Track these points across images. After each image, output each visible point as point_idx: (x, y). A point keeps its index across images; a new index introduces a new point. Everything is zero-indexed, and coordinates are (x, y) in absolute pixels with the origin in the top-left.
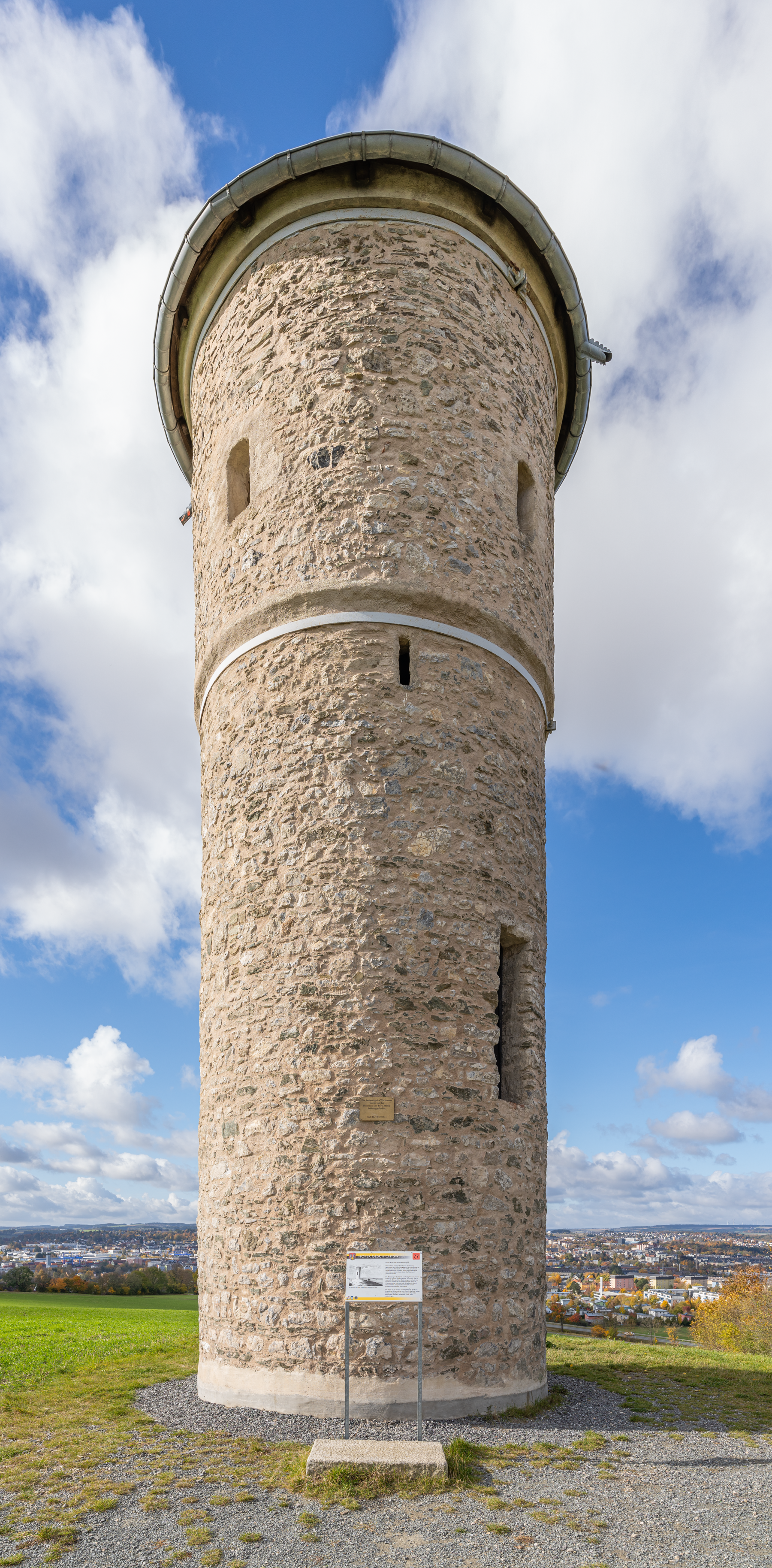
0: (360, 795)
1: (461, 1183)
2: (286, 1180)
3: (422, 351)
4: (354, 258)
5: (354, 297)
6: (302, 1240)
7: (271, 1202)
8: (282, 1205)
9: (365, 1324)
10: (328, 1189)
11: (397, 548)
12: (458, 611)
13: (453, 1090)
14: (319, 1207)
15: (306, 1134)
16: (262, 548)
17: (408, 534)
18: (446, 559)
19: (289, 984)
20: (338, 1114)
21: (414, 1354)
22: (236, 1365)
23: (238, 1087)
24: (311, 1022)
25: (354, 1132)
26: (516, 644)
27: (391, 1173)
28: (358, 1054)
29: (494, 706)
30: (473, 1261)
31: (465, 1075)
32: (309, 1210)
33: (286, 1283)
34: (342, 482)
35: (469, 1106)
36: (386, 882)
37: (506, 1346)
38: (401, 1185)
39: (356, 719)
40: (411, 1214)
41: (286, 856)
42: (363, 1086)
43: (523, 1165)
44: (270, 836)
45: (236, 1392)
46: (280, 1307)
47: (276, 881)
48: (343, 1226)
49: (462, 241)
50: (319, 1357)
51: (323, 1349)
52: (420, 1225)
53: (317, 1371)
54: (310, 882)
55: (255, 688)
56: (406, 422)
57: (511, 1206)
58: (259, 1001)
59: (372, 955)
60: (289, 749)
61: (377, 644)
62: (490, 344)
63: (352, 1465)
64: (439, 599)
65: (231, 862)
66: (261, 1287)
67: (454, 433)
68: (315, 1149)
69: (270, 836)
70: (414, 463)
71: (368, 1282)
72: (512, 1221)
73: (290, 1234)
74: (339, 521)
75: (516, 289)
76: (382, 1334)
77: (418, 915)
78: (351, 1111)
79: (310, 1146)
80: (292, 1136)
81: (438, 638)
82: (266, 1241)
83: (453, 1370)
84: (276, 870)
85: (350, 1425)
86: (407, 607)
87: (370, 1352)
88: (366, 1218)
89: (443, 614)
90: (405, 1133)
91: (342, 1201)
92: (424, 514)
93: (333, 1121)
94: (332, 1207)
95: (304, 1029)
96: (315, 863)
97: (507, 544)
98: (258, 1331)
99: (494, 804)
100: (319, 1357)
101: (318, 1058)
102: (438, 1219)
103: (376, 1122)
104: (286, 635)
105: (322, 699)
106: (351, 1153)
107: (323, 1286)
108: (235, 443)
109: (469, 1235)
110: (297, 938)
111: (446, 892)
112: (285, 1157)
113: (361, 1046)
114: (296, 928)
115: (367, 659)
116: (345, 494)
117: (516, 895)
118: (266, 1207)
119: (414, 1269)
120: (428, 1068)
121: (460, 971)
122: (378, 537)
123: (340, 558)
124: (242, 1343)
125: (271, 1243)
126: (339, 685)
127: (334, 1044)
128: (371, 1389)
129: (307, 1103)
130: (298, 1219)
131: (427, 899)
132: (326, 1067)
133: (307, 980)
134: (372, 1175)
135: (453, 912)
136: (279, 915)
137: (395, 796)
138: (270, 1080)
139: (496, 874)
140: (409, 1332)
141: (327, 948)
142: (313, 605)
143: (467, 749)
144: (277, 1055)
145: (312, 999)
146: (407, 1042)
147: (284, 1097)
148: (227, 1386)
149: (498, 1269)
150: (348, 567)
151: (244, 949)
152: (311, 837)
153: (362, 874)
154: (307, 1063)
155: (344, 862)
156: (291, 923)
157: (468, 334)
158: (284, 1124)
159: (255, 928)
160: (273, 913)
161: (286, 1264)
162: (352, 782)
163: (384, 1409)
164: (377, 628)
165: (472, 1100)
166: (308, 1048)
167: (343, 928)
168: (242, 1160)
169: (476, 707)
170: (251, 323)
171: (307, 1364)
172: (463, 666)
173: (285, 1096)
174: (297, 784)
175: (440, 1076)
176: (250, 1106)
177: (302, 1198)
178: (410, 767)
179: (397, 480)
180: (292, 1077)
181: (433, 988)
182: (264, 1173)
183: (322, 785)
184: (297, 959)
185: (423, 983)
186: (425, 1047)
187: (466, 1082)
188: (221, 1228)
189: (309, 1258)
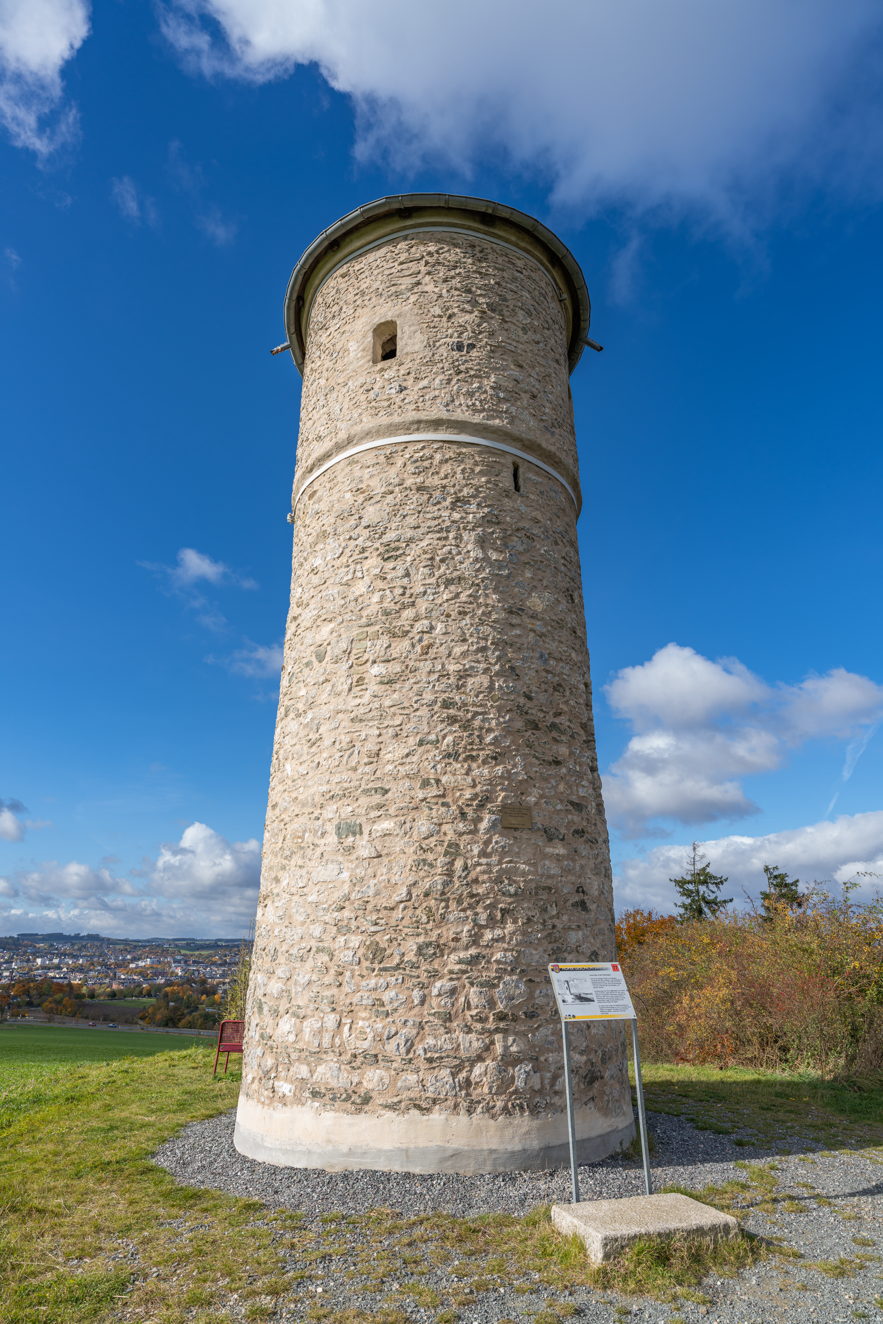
1: (583, 892)
3: (522, 312)
6: (442, 951)
7: (405, 908)
8: (418, 912)
9: (514, 1049)
10: (472, 896)
11: (513, 409)
12: (549, 456)
13: (572, 803)
14: (462, 914)
15: (449, 838)
16: (409, 383)
17: (519, 403)
18: (542, 424)
19: (428, 697)
20: (481, 819)
23: (363, 787)
24: (451, 732)
25: (496, 838)
28: (496, 765)
31: (578, 791)
32: (451, 917)
33: (423, 1002)
34: (475, 363)
36: (513, 626)
38: (540, 892)
39: (485, 506)
41: (425, 593)
42: (503, 794)
44: (407, 575)
45: (344, 1149)
46: (415, 1032)
47: (414, 611)
48: (488, 935)
49: (539, 269)
50: (463, 1092)
51: (468, 1082)
52: (557, 935)
53: (462, 1112)
54: (448, 616)
56: (514, 344)
58: (392, 709)
59: (504, 682)
60: (429, 516)
61: (499, 462)
64: (539, 446)
65: (360, 588)
66: (389, 1008)
68: (457, 854)
69: (407, 575)
70: (521, 367)
71: (581, 998)
73: (430, 944)
74: (472, 384)
75: (560, 301)
76: (531, 1059)
77: (538, 655)
78: (494, 817)
79: (453, 851)
80: (433, 839)
81: (537, 469)
82: (396, 953)
83: (593, 1099)
84: (414, 602)
87: (519, 1083)
88: (510, 927)
89: (540, 455)
91: (486, 908)
93: (476, 826)
94: (476, 914)
95: (444, 737)
96: (453, 602)
100: (463, 1092)
101: (459, 765)
102: (570, 928)
104: (428, 441)
105: (457, 487)
106: (495, 859)
108: (383, 320)
110: (436, 658)
111: (554, 640)
112: (424, 860)
113: (499, 758)
114: (435, 651)
115: (490, 470)
116: (476, 370)
118: (398, 914)
119: (618, 982)
120: (553, 782)
121: (566, 702)
122: (500, 400)
123: (474, 405)
124: (356, 1080)
125: (403, 954)
126: (472, 482)
127: (474, 753)
128: (524, 1130)
129: (449, 807)
130: (438, 927)
131: (541, 643)
132: (467, 774)
133: (447, 695)
134: (515, 882)
136: (417, 638)
137: (515, 564)
141: (466, 670)
142: (451, 427)
143: (556, 544)
144: (415, 759)
145: (452, 711)
146: (537, 758)
148: (329, 1141)
151: (374, 662)
152: (449, 582)
153: (494, 616)
154: (448, 769)
155: (479, 606)
156: (430, 646)
158: (423, 826)
159: (390, 646)
160: (411, 635)
161: (424, 978)
162: (482, 548)
163: (538, 1155)
164: (499, 452)
166: (449, 756)
168: (366, 863)
170: (401, 263)
171: (450, 1103)
173: (425, 799)
174: (436, 542)
175: (562, 790)
176: (380, 807)
177: (443, 904)
178: (525, 546)
180: (433, 781)
181: (551, 713)
182: (398, 875)
183: (458, 546)
184: (436, 676)
185: (544, 709)
186: (550, 764)
187: (579, 797)
188: (327, 937)
189: (451, 972)
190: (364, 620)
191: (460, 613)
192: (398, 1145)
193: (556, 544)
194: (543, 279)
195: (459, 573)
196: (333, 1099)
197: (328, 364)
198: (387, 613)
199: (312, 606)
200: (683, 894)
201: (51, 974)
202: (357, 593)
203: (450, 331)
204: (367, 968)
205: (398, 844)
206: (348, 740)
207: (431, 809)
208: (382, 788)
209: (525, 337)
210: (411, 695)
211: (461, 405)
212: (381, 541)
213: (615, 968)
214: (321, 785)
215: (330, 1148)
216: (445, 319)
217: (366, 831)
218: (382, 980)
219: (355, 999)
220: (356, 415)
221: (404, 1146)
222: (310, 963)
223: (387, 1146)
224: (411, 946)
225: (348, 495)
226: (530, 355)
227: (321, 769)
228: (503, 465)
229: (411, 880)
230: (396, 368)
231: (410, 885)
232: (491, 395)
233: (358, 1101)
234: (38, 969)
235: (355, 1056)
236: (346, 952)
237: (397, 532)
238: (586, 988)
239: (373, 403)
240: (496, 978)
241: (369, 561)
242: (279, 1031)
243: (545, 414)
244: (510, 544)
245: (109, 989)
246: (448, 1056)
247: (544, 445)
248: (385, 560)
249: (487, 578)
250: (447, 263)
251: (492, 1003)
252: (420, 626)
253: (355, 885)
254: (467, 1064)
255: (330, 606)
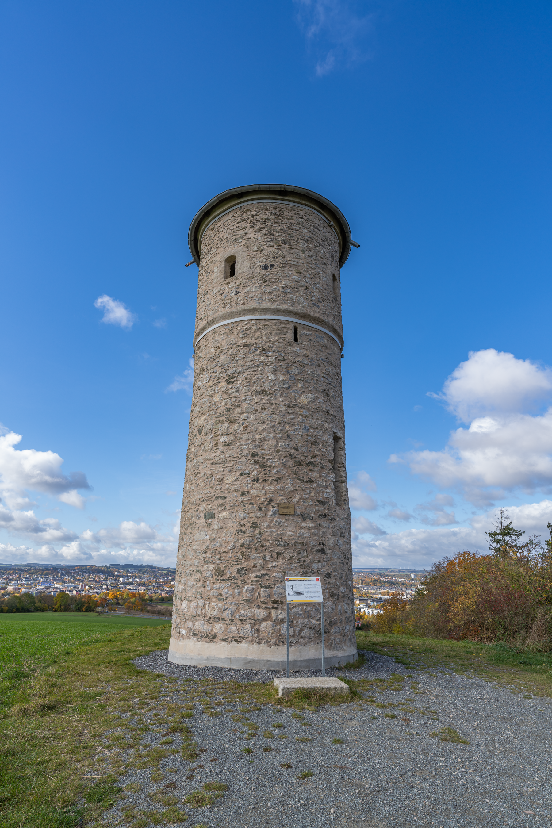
0: (279, 379)
1: (323, 544)
2: (241, 541)
3: (302, 241)
4: (278, 213)
5: (278, 223)
9: (281, 617)
16: (240, 290)
17: (298, 294)
18: (311, 303)
19: (246, 452)
20: (268, 510)
21: (305, 632)
22: (206, 641)
23: (216, 496)
24: (256, 469)
26: (334, 330)
27: (293, 539)
29: (327, 351)
30: (329, 583)
31: (323, 495)
32: (253, 557)
33: (239, 595)
35: (325, 509)
36: (290, 413)
37: (344, 628)
40: (302, 559)
41: (246, 399)
43: (346, 536)
45: (205, 657)
46: (235, 608)
47: (240, 409)
49: (314, 213)
51: (258, 630)
54: (257, 410)
55: (233, 336)
56: (297, 260)
57: (342, 556)
58: (229, 458)
60: (249, 360)
62: (323, 241)
63: (304, 689)
64: (309, 316)
65: (216, 398)
66: (224, 597)
67: (313, 265)
69: (238, 391)
70: (300, 273)
71: (297, 593)
72: (343, 563)
74: (272, 287)
80: (245, 520)
81: (308, 327)
85: (295, 669)
86: (297, 316)
88: (281, 561)
90: (299, 520)
92: (303, 288)
95: (253, 471)
97: (331, 299)
98: (221, 621)
99: (329, 386)
102: (314, 562)
103: (286, 515)
106: (274, 529)
107: (259, 596)
108: (229, 256)
109: (327, 570)
112: (241, 530)
115: (281, 332)
117: (337, 420)
118: (229, 555)
119: (318, 586)
121: (319, 450)
124: (210, 628)
130: (247, 561)
135: (316, 427)
136: (241, 422)
138: (235, 494)
139: (331, 412)
140: (302, 620)
143: (319, 366)
144: (238, 482)
145: (256, 459)
146: (299, 480)
147: (242, 502)
148: (199, 654)
149: (339, 588)
150: (275, 302)
151: (222, 435)
152: (257, 393)
156: (247, 426)
157: (316, 238)
160: (238, 421)
162: (275, 374)
165: (326, 506)
166: (254, 480)
167: (271, 431)
169: (322, 351)
170: (238, 223)
172: (317, 337)
174: (252, 373)
176: (222, 505)
177: (249, 551)
178: (299, 371)
179: (294, 277)
180: (246, 493)
181: (309, 457)
184: (250, 442)
185: (305, 455)
186: (307, 482)
187: (324, 498)
188: (200, 565)
189: (252, 581)
190: (218, 414)
191: (262, 409)
192: (227, 656)
193: (319, 366)
194: (318, 218)
195: (263, 388)
196: (201, 636)
197: (206, 278)
198: (228, 410)
199: (197, 406)
200: (494, 542)
201: (128, 587)
202: (216, 400)
203: (262, 259)
204: (216, 579)
205: (229, 523)
206: (210, 473)
207: (245, 506)
208: (223, 496)
209: (303, 255)
210: (238, 451)
211: (265, 299)
212: (226, 373)
213: (317, 580)
214: (199, 495)
215: (200, 657)
216: (259, 252)
217: (216, 517)
218: (222, 585)
219: (211, 593)
220: (216, 308)
221: (229, 657)
222: (193, 577)
223: (222, 657)
224: (235, 569)
225: (213, 350)
226: (305, 264)
227: (199, 487)
228: (288, 328)
229: (235, 539)
230: (234, 281)
231: (234, 542)
232: (282, 292)
233: (211, 637)
234: (121, 584)
235: (210, 618)
236: (207, 572)
237: (234, 369)
238: (301, 588)
239: (224, 301)
240: (273, 584)
241: (221, 384)
242: (182, 607)
243: (313, 296)
244: (290, 370)
245: (160, 596)
246: (249, 619)
247: (312, 314)
248: (228, 383)
249: (277, 390)
250: (261, 220)
251: (270, 596)
252: (242, 417)
253: (211, 542)
254: (258, 622)
255: (204, 406)
